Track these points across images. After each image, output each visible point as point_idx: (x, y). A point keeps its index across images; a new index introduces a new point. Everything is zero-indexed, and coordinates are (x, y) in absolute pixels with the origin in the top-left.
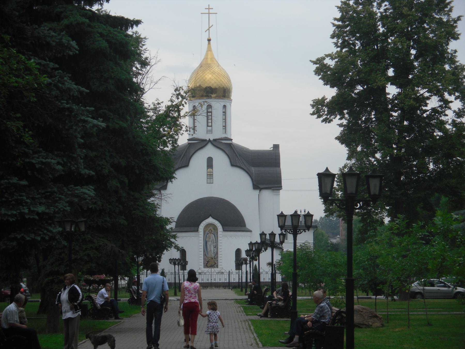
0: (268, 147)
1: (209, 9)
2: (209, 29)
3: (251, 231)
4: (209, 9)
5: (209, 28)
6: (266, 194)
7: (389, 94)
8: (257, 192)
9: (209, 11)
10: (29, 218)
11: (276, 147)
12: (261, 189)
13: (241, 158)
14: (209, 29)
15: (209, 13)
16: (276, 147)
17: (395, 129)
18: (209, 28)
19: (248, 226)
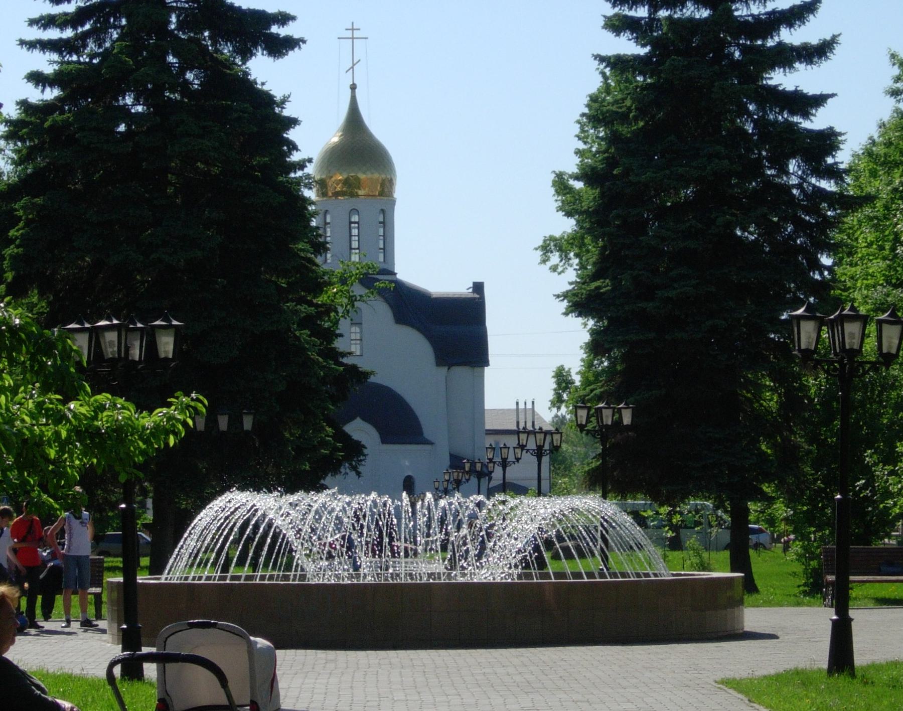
0: (460, 287)
1: (353, 29)
2: (352, 68)
3: (432, 444)
4: (353, 29)
5: (354, 65)
6: (461, 372)
7: (834, 157)
8: (444, 370)
9: (353, 34)
10: (82, 26)
11: (478, 287)
12: (450, 366)
13: (411, 306)
14: (352, 68)
15: (353, 38)
16: (478, 287)
17: (23, 341)
18: (354, 65)
19: (427, 433)
